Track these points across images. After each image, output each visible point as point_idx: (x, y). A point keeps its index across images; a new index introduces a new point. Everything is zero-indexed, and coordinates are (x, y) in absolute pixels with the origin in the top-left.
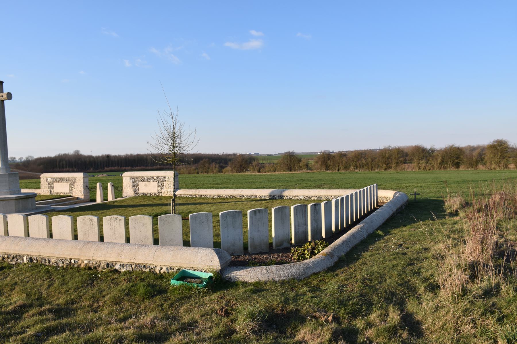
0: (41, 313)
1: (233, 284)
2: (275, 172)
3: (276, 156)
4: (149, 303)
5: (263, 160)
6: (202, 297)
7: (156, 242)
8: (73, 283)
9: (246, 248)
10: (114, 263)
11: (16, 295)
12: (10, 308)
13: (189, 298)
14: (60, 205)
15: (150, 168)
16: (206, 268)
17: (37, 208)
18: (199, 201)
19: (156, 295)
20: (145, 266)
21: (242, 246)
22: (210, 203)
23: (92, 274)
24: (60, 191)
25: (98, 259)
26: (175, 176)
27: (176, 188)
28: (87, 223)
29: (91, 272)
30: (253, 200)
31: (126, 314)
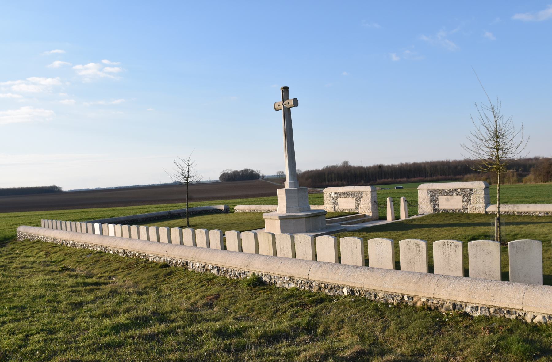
7: (505, 277)
8: (414, 328)
10: (463, 304)
11: (345, 335)
14: (347, 224)
15: (429, 178)
17: (328, 227)
18: (519, 220)
20: (508, 312)
23: (436, 317)
24: (344, 208)
25: (441, 297)
26: (486, 189)
27: (487, 204)
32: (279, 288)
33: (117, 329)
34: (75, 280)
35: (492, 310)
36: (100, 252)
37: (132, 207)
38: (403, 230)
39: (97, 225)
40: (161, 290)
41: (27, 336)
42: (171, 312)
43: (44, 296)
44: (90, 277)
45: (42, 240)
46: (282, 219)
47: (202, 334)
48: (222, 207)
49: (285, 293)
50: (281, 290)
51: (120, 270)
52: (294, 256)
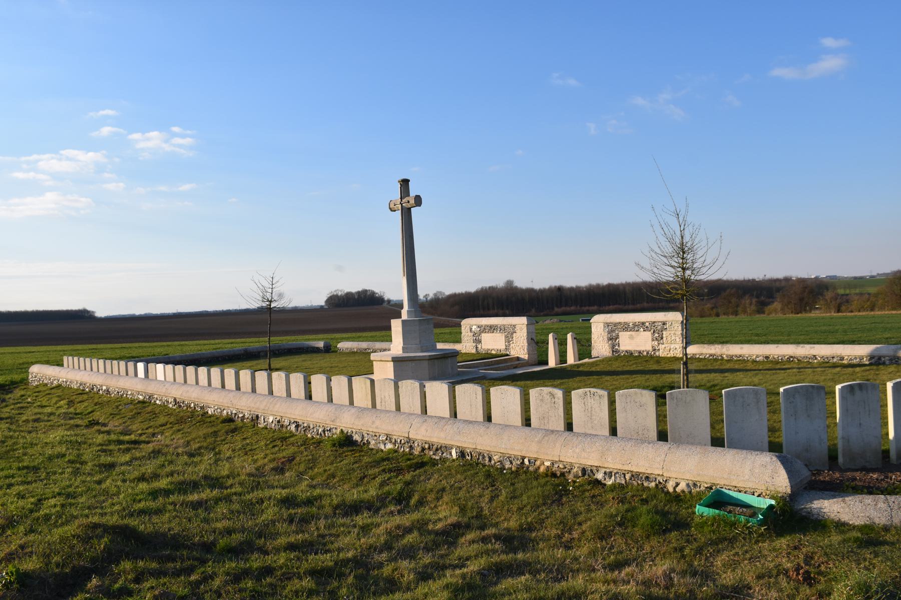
0: (484, 540)
1: (818, 525)
2: (872, 310)
3: (872, 280)
4: (659, 542)
5: (845, 288)
6: (757, 542)
7: (662, 436)
8: (529, 497)
9: (833, 457)
11: (444, 506)
12: (439, 526)
13: (732, 541)
14: (491, 369)
15: (631, 307)
16: (761, 488)
18: (728, 366)
19: (670, 531)
20: (647, 478)
21: (826, 452)
22: (751, 370)
23: (558, 485)
24: (490, 347)
25: (568, 460)
28: (546, 399)
29: (557, 481)
30: (835, 366)
31: (620, 557)
32: (372, 449)
33: (154, 494)
34: (106, 437)
35: (628, 476)
36: (143, 402)
37: (195, 342)
38: (562, 379)
39: (141, 366)
40: (220, 451)
41: (40, 500)
42: (228, 477)
43: (64, 456)
44: (126, 435)
45: (64, 385)
46: (396, 360)
47: (263, 502)
48: (321, 344)
49: (380, 455)
50: (374, 452)
51: (168, 426)
52: (398, 408)
